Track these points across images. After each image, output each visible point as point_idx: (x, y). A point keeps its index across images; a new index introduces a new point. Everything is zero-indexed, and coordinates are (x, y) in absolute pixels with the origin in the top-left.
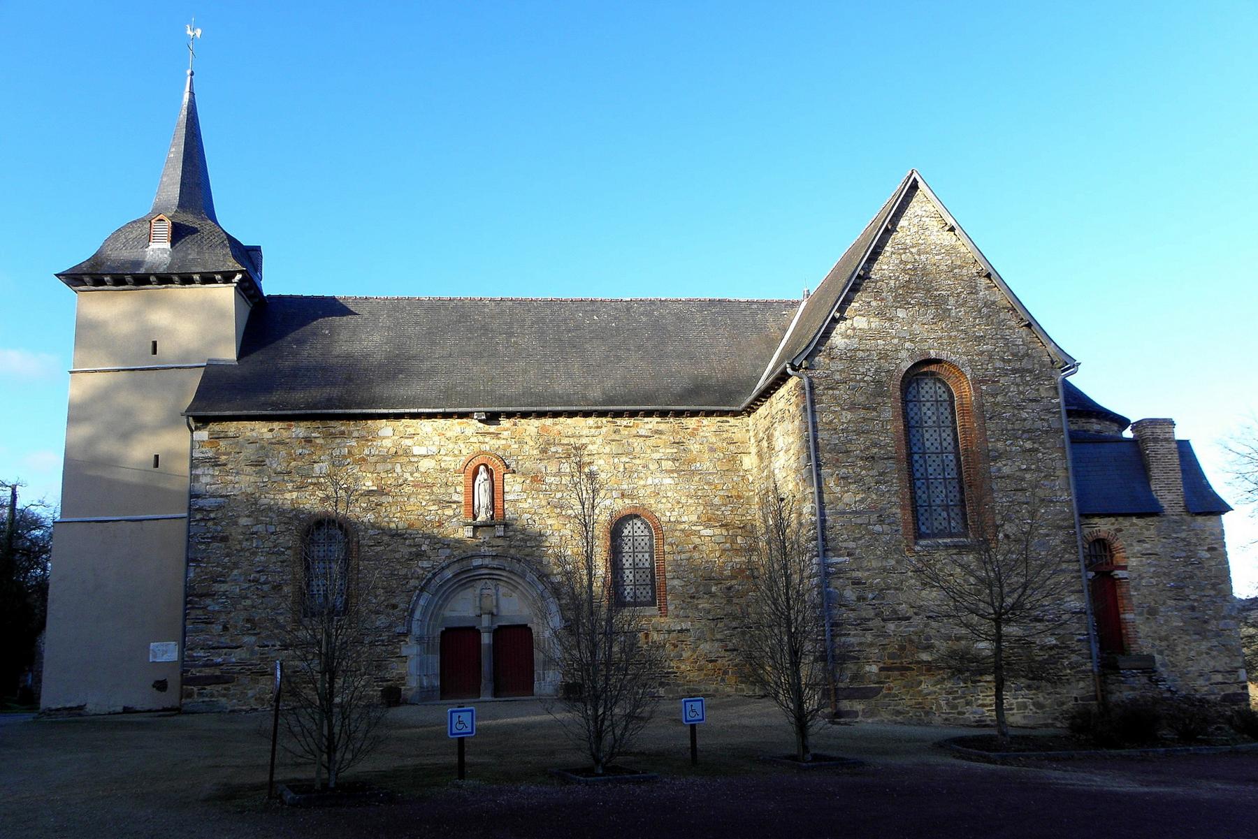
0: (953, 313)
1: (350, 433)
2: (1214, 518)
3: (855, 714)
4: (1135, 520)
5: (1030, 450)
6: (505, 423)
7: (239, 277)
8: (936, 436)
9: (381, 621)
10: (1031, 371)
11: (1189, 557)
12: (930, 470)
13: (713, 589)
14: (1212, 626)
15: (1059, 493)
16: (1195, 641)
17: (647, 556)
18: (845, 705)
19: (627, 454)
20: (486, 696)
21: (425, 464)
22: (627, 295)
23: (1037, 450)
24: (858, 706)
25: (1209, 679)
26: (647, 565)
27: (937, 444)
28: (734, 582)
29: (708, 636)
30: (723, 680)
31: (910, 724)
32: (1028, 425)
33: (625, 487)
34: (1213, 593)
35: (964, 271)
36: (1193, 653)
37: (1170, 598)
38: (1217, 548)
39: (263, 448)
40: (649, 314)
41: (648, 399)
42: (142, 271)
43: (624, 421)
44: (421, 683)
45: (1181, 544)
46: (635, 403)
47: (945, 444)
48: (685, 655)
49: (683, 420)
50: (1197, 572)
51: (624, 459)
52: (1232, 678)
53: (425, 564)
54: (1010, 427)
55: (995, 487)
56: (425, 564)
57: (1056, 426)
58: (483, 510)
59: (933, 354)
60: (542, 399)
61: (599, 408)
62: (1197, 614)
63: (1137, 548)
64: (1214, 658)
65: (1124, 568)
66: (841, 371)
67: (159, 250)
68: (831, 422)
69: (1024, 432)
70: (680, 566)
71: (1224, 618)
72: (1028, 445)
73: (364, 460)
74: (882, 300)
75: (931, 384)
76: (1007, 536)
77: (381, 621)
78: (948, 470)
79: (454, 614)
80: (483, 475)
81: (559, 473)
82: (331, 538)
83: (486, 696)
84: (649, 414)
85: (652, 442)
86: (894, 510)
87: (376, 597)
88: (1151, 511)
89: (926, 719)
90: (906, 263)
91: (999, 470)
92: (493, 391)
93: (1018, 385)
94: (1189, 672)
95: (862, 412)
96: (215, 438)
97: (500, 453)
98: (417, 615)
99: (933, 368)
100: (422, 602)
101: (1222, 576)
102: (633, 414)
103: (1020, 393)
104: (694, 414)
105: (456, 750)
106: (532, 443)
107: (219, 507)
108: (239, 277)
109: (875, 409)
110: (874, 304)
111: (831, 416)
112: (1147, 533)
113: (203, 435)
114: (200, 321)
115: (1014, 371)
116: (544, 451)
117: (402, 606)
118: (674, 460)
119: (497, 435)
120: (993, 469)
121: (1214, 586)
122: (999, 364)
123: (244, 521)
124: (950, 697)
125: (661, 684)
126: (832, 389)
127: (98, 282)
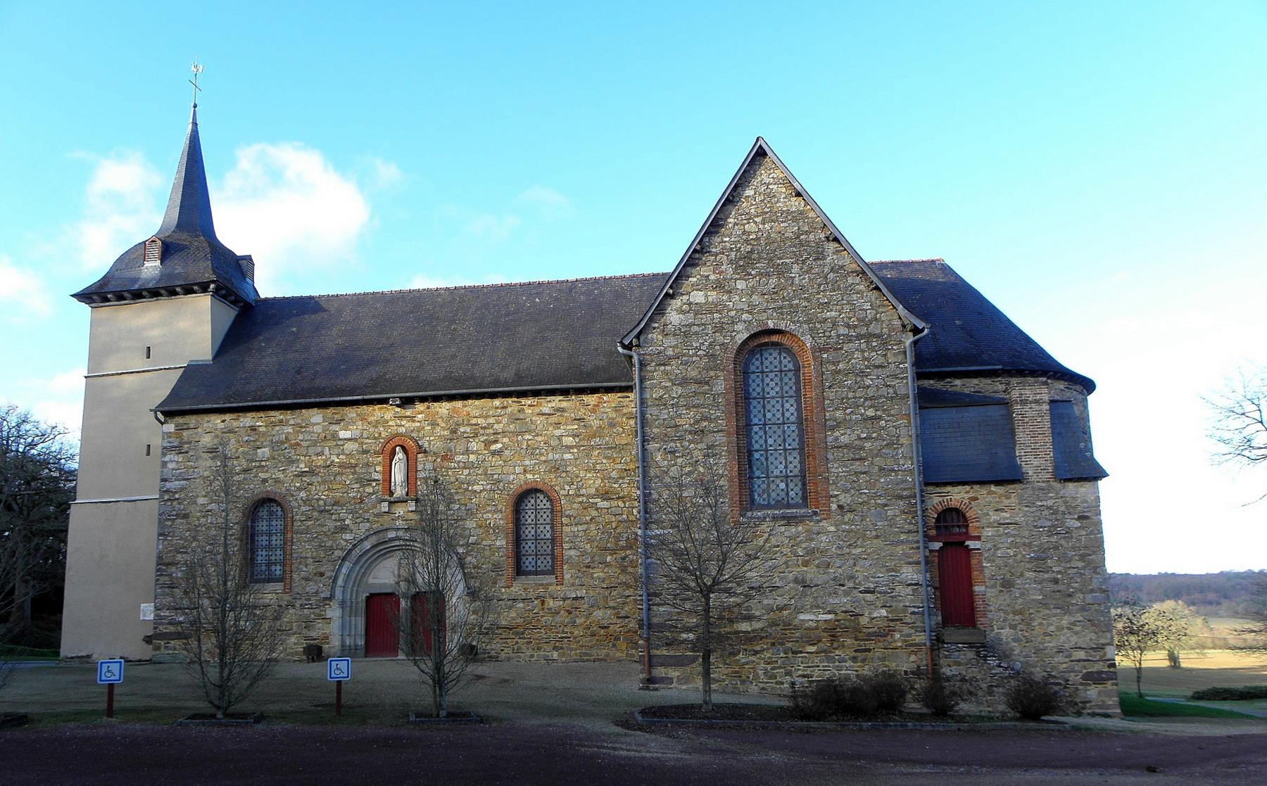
0: (797, 281)
1: (288, 421)
2: (1088, 485)
3: (670, 680)
4: (993, 488)
5: (872, 418)
6: (420, 407)
7: (212, 286)
8: (778, 406)
9: (311, 588)
10: (878, 336)
11: (1055, 527)
12: (770, 441)
13: (609, 559)
14: (1078, 599)
15: (901, 462)
16: (1055, 615)
17: (548, 527)
18: (660, 672)
19: (529, 432)
20: (401, 656)
21: (350, 447)
22: (396, 288)
23: (880, 418)
24: (674, 673)
25: (1070, 656)
26: (548, 536)
27: (779, 415)
28: (628, 552)
29: (601, 603)
30: (614, 645)
31: (724, 692)
32: (871, 392)
33: (527, 463)
34: (1080, 564)
35: (811, 237)
36: (1052, 628)
37: (1030, 570)
38: (1090, 518)
39: (217, 436)
40: (588, 293)
41: (589, 376)
42: (136, 287)
43: (529, 401)
44: (343, 641)
45: (1046, 512)
46: (532, 384)
47: (787, 414)
48: (578, 621)
49: (584, 397)
50: (1063, 542)
51: (527, 437)
52: (1098, 656)
53: (348, 536)
54: (851, 394)
55: (830, 456)
56: (348, 536)
57: (902, 391)
58: (398, 488)
59: (771, 325)
60: (458, 382)
61: (605, 384)
62: (1061, 587)
63: (994, 517)
64: (1076, 633)
65: (978, 538)
66: (676, 346)
67: (152, 267)
68: (661, 397)
69: (866, 399)
70: (577, 536)
71: (1092, 591)
72: (871, 413)
73: (298, 444)
74: (720, 273)
75: (775, 354)
76: (841, 507)
77: (311, 588)
78: (789, 440)
79: (376, 581)
80: (400, 455)
81: (467, 452)
82: (271, 514)
83: (401, 656)
84: (552, 392)
85: (553, 419)
86: (721, 483)
87: (306, 566)
88: (1011, 477)
89: (741, 688)
90: (749, 233)
91: (837, 439)
92: (417, 377)
93: (863, 351)
94: (1045, 649)
95: (694, 387)
96: (180, 429)
97: (414, 435)
98: (340, 582)
99: (775, 338)
100: (344, 570)
101: (1096, 546)
102: (536, 394)
103: (865, 359)
104: (594, 391)
105: (106, 698)
106: (443, 425)
107: (182, 489)
108: (212, 286)
109: (707, 383)
110: (712, 277)
111: (662, 392)
112: (1006, 502)
113: (170, 427)
114: (192, 326)
115: (859, 337)
116: (454, 432)
117: (328, 574)
118: (574, 436)
119: (412, 419)
120: (830, 439)
121: (1082, 557)
122: (842, 331)
123: (201, 501)
124: (769, 667)
125: (555, 648)
126: (665, 365)
127: (172, 293)
